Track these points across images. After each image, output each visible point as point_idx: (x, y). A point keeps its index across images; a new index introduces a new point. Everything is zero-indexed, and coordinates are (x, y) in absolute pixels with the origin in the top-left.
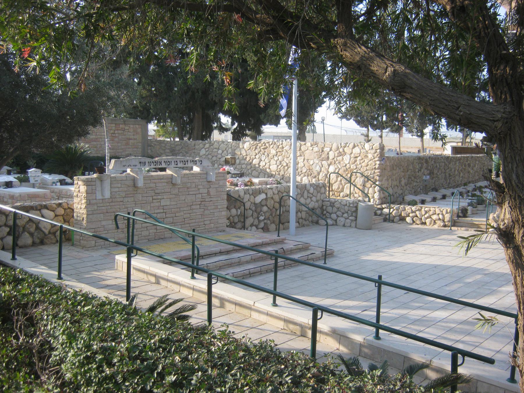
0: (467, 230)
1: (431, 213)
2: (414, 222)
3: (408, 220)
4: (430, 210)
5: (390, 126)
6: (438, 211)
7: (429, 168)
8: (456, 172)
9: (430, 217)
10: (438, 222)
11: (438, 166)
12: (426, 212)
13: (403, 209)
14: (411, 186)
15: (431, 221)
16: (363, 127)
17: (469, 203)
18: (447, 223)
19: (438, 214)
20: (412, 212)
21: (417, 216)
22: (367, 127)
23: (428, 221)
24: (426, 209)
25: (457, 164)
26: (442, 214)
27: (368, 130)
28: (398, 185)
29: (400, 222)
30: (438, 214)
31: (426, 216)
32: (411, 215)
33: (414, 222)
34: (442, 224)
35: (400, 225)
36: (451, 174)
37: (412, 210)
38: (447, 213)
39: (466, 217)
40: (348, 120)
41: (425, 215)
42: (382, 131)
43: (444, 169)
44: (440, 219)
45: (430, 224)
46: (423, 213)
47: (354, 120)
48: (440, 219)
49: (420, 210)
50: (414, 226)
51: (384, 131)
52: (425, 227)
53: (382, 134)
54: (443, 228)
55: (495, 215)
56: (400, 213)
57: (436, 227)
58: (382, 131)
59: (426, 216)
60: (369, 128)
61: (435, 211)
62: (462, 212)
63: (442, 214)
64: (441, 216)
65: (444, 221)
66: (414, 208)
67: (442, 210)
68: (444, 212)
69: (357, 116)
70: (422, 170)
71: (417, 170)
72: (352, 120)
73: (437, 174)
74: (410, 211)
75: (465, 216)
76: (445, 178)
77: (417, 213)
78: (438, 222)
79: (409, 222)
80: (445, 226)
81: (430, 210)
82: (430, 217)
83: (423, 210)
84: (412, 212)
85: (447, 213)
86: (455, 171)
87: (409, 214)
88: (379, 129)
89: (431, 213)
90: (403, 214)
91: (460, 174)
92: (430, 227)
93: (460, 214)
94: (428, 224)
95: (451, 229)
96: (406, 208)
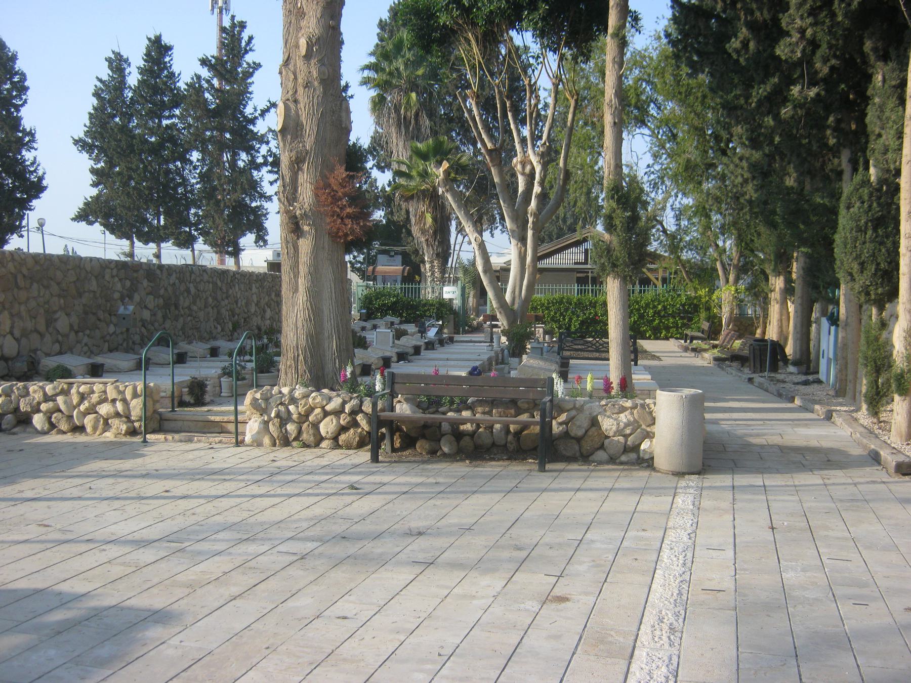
0: (190, 440)
1: (95, 398)
2: (53, 426)
3: (38, 420)
4: (93, 392)
5: (173, 234)
6: (111, 393)
7: (162, 292)
8: (253, 309)
9: (92, 410)
10: (114, 422)
11: (193, 290)
12: (83, 397)
13: (22, 392)
14: (98, 333)
15: (97, 421)
16: (121, 238)
17: (224, 369)
18: (137, 424)
19: (114, 401)
20: (47, 398)
21: (60, 411)
22: (129, 238)
23: (88, 421)
24: (82, 389)
25: (254, 290)
26: (124, 400)
27: (133, 243)
28: (42, 327)
29: (15, 430)
30: (114, 401)
31: (82, 408)
32: (43, 407)
33: (53, 426)
34: (124, 427)
35: (15, 437)
36: (237, 311)
37: (45, 394)
38: (135, 395)
39: (203, 404)
40: (91, 223)
41: (79, 405)
42: (159, 246)
43: (215, 299)
44: (117, 415)
45: (95, 428)
46: (75, 399)
47: (101, 224)
48: (117, 415)
49: (66, 392)
50: (53, 438)
51: (163, 245)
52: (80, 438)
53: (159, 251)
54: (128, 439)
55: (258, 396)
56: (12, 406)
57: (109, 436)
58: (159, 246)
59: (82, 408)
60: (135, 240)
61: (105, 392)
62: (191, 392)
63: (124, 400)
64: (119, 406)
65: (128, 417)
66: (49, 388)
67: (121, 388)
68: (128, 396)
69: (106, 216)
70: (137, 297)
71: (117, 295)
72: (97, 225)
73: (189, 308)
74: (38, 396)
75: (199, 402)
76: (217, 320)
77: (60, 399)
78: (114, 422)
79: (39, 427)
80: (133, 432)
81: (93, 392)
82: (92, 410)
83: (74, 391)
84: (47, 398)
85: (135, 395)
86: (247, 304)
87: (39, 404)
88: (154, 242)
89: (95, 398)
90: (24, 407)
91: (264, 311)
92: (96, 438)
93: (187, 398)
94: (89, 429)
95: (145, 441)
96: (31, 389)
